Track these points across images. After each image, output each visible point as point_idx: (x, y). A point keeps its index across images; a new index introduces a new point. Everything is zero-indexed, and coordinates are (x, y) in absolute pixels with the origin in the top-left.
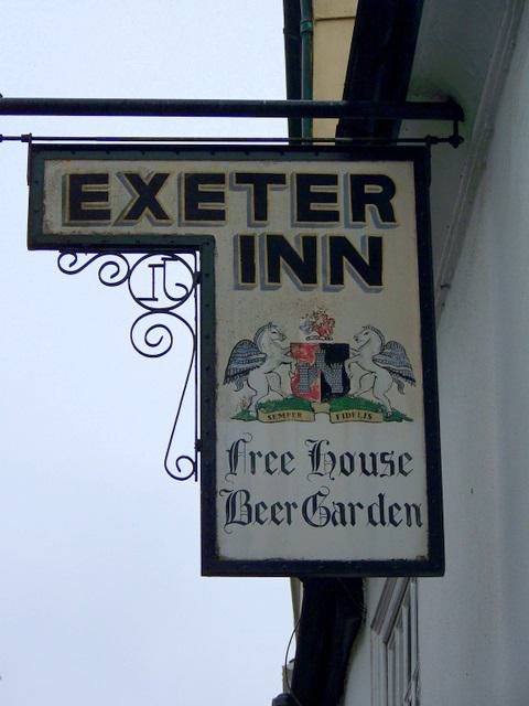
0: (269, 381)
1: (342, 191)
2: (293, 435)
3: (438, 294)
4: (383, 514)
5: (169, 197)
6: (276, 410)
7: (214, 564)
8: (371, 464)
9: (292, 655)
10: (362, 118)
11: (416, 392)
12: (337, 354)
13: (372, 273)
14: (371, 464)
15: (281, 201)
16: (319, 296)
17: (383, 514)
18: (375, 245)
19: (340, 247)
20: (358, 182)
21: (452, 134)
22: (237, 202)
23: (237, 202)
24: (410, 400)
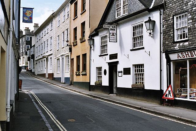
0: (111, 34)
5: (108, 26)
12: (114, 33)
15: (112, 27)
22: (110, 27)
24: (116, 35)
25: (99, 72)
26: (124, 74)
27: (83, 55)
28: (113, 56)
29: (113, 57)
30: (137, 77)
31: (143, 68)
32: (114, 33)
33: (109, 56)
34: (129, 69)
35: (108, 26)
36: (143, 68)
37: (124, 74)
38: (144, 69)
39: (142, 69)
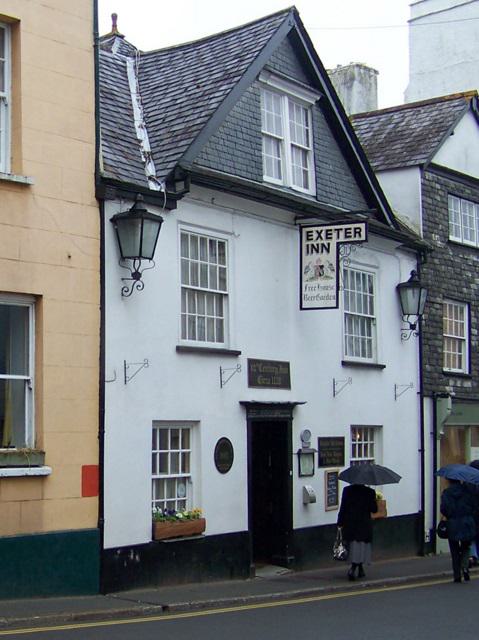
0: (311, 273)
1: (352, 231)
2: (314, 283)
3: (329, 140)
4: (328, 297)
5: (323, 235)
6: (312, 279)
7: (301, 309)
8: (326, 288)
9: (274, 572)
10: (146, 146)
11: (335, 273)
12: (322, 267)
13: (328, 251)
14: (326, 288)
15: (342, 234)
16: (319, 255)
17: (328, 297)
18: (329, 244)
19: (323, 245)
20: (355, 229)
21: (416, 511)
22: (334, 235)
23: (334, 235)
24: (334, 275)
25: (360, 445)
26: (342, 439)
27: (253, 382)
28: (273, 369)
29: (266, 375)
30: (170, 451)
31: (369, 442)
32: (322, 267)
33: (243, 361)
34: (277, 414)
35: (323, 235)
36: (158, 451)
37: (342, 439)
38: (154, 448)
39: (163, 446)
